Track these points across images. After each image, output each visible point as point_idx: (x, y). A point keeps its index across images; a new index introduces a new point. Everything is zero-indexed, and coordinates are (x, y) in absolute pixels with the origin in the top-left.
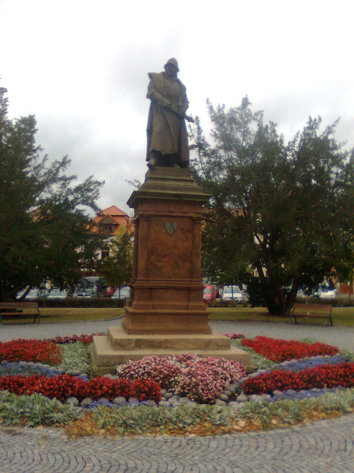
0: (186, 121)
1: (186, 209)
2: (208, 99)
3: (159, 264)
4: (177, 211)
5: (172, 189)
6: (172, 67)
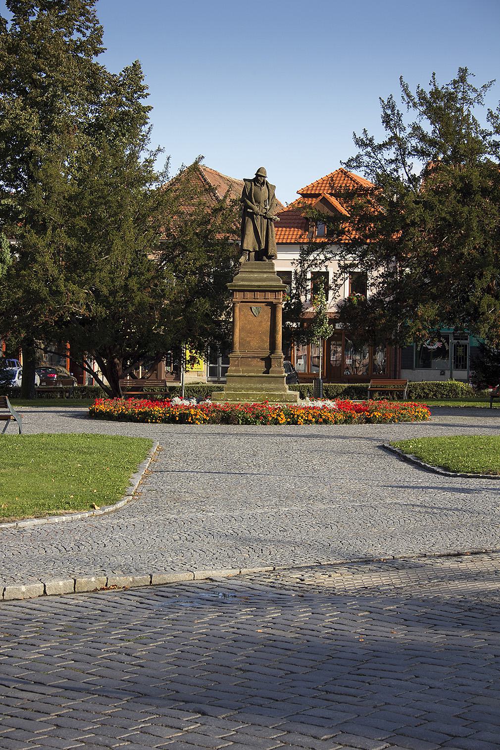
1: (269, 295)
2: (401, 77)
3: (248, 339)
4: (260, 296)
5: (257, 281)
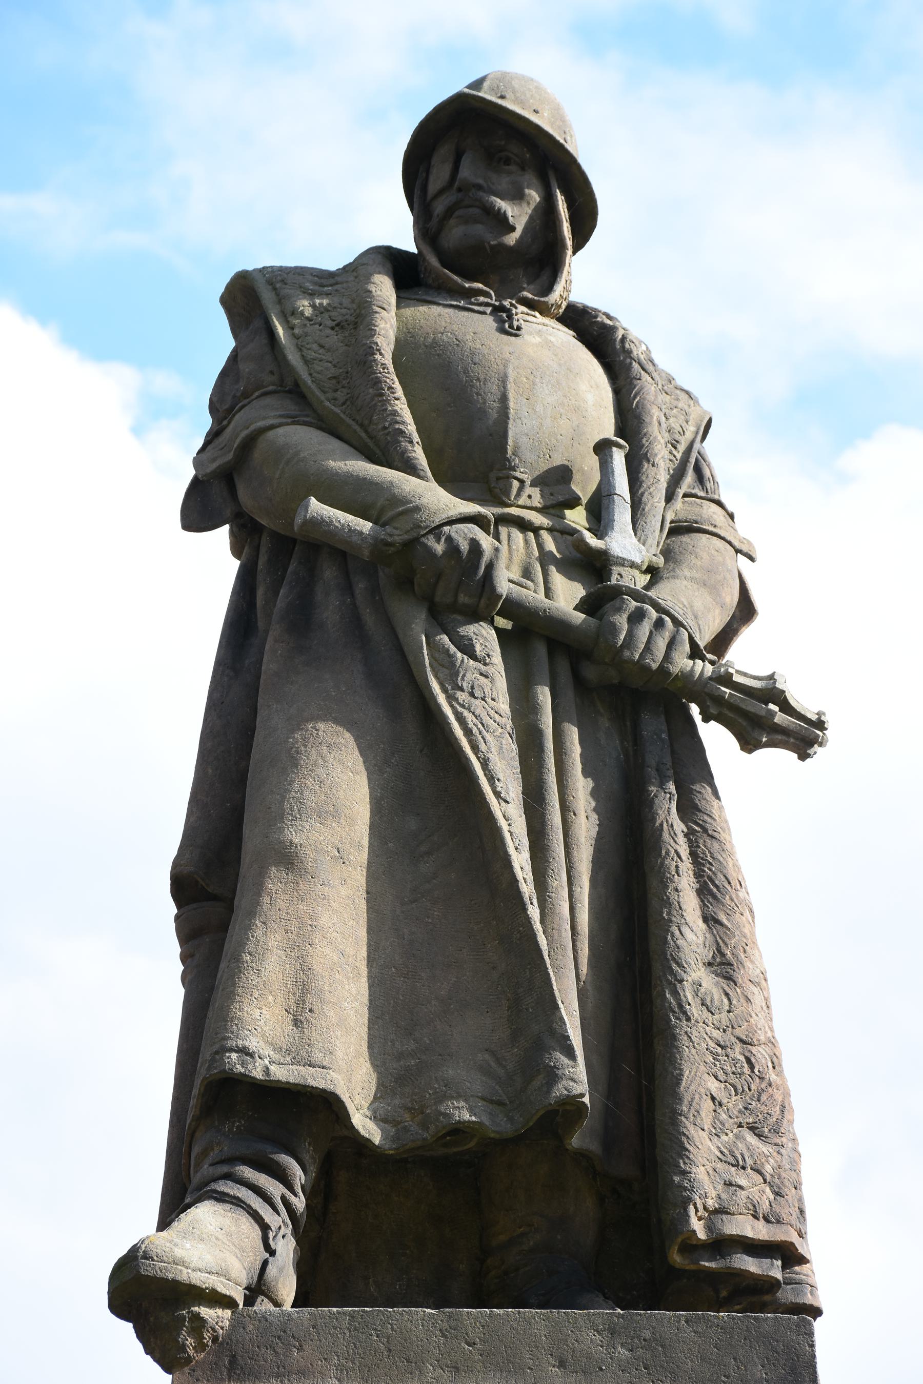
0: (716, 739)
6: (492, 187)
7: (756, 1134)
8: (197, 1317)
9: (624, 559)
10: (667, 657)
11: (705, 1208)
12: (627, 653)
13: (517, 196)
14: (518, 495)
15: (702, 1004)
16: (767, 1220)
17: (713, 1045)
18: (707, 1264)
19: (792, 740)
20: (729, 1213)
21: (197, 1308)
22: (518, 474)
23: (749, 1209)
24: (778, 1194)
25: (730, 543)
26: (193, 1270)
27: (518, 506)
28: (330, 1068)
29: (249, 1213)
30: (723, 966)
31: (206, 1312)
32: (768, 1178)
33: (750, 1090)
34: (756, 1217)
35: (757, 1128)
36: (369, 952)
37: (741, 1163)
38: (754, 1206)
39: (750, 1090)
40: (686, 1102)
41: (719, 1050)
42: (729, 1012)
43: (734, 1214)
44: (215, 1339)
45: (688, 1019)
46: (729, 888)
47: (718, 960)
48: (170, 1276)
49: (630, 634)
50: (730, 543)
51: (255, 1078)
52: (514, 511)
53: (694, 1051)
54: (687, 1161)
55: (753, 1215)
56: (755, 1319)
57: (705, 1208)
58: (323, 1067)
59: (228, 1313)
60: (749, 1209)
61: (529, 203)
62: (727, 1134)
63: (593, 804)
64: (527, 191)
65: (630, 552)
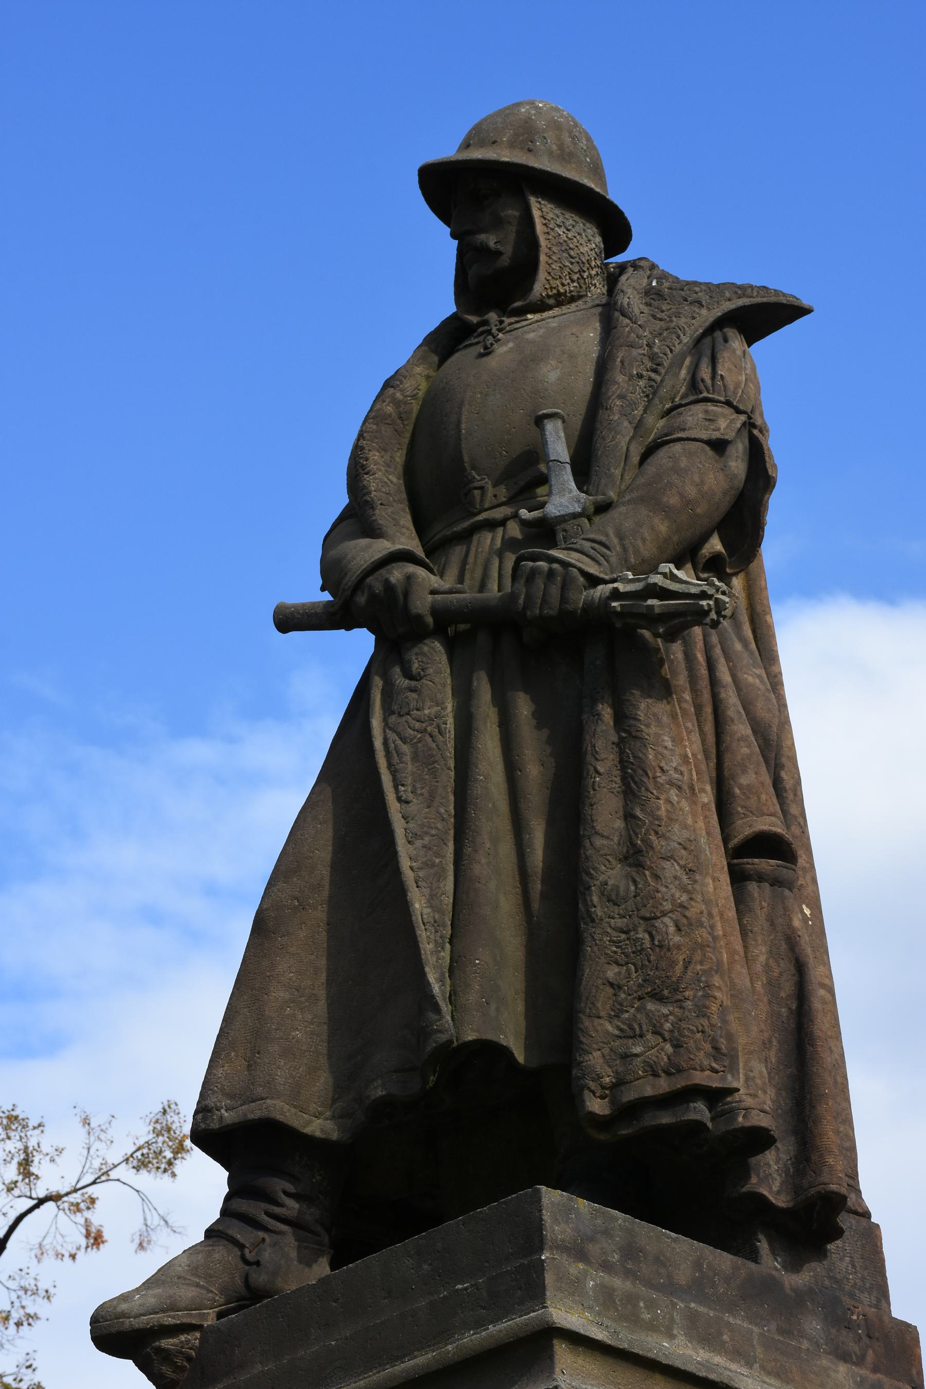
7: (657, 1000)
8: (159, 1350)
9: (563, 516)
10: (563, 599)
11: (603, 1088)
12: (529, 613)
13: (498, 223)
14: (482, 501)
15: (608, 901)
16: (668, 1073)
17: (614, 933)
18: (624, 1132)
19: (689, 618)
20: (627, 1083)
21: (157, 1343)
22: (476, 484)
23: (647, 1072)
24: (677, 1046)
25: (695, 440)
26: (135, 1318)
27: (486, 510)
28: (267, 1098)
29: (228, 1240)
30: (634, 856)
31: (167, 1343)
32: (667, 1035)
33: (649, 961)
34: (656, 1075)
35: (657, 994)
36: (328, 976)
37: (638, 1031)
38: (651, 1067)
39: (649, 961)
40: (584, 999)
41: (623, 936)
42: (635, 897)
43: (631, 1082)
44: (189, 1359)
45: (593, 921)
46: (645, 780)
47: (631, 852)
48: (113, 1330)
49: (528, 597)
50: (695, 440)
51: (212, 1129)
52: (480, 517)
53: (595, 949)
54: (581, 1052)
55: (652, 1075)
56: (505, 1203)
57: (603, 1088)
58: (262, 1099)
59: (198, 1335)
60: (647, 1072)
61: (509, 223)
62: (627, 1012)
63: (549, 750)
64: (502, 214)
65: (568, 507)
